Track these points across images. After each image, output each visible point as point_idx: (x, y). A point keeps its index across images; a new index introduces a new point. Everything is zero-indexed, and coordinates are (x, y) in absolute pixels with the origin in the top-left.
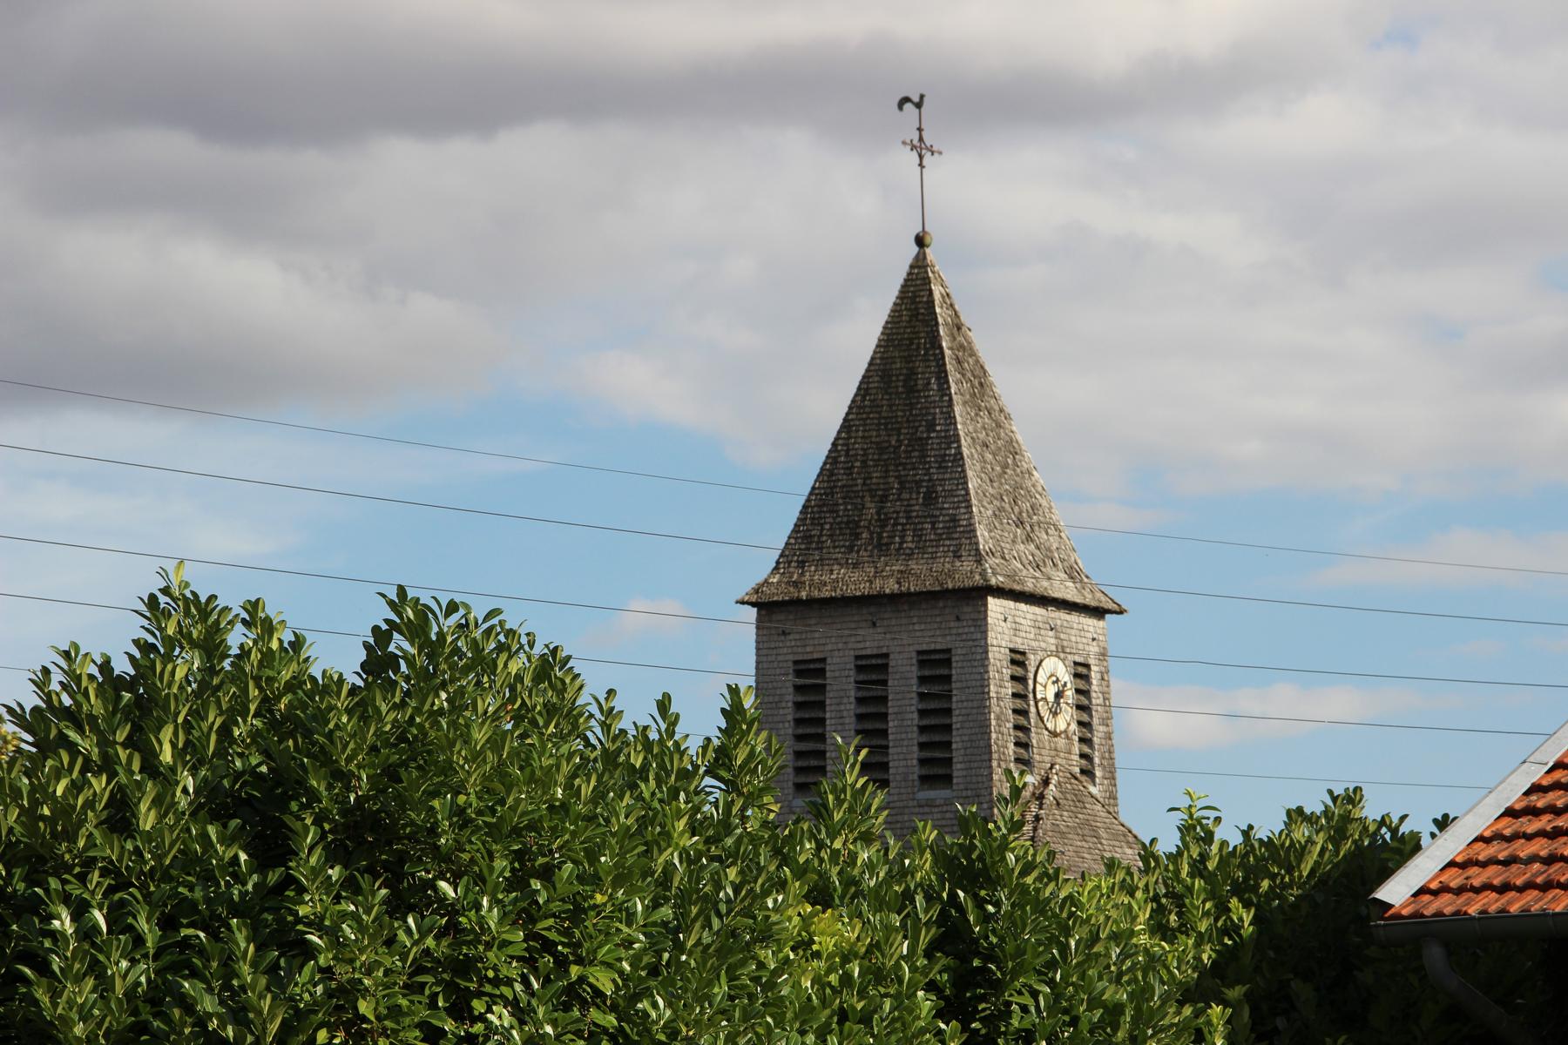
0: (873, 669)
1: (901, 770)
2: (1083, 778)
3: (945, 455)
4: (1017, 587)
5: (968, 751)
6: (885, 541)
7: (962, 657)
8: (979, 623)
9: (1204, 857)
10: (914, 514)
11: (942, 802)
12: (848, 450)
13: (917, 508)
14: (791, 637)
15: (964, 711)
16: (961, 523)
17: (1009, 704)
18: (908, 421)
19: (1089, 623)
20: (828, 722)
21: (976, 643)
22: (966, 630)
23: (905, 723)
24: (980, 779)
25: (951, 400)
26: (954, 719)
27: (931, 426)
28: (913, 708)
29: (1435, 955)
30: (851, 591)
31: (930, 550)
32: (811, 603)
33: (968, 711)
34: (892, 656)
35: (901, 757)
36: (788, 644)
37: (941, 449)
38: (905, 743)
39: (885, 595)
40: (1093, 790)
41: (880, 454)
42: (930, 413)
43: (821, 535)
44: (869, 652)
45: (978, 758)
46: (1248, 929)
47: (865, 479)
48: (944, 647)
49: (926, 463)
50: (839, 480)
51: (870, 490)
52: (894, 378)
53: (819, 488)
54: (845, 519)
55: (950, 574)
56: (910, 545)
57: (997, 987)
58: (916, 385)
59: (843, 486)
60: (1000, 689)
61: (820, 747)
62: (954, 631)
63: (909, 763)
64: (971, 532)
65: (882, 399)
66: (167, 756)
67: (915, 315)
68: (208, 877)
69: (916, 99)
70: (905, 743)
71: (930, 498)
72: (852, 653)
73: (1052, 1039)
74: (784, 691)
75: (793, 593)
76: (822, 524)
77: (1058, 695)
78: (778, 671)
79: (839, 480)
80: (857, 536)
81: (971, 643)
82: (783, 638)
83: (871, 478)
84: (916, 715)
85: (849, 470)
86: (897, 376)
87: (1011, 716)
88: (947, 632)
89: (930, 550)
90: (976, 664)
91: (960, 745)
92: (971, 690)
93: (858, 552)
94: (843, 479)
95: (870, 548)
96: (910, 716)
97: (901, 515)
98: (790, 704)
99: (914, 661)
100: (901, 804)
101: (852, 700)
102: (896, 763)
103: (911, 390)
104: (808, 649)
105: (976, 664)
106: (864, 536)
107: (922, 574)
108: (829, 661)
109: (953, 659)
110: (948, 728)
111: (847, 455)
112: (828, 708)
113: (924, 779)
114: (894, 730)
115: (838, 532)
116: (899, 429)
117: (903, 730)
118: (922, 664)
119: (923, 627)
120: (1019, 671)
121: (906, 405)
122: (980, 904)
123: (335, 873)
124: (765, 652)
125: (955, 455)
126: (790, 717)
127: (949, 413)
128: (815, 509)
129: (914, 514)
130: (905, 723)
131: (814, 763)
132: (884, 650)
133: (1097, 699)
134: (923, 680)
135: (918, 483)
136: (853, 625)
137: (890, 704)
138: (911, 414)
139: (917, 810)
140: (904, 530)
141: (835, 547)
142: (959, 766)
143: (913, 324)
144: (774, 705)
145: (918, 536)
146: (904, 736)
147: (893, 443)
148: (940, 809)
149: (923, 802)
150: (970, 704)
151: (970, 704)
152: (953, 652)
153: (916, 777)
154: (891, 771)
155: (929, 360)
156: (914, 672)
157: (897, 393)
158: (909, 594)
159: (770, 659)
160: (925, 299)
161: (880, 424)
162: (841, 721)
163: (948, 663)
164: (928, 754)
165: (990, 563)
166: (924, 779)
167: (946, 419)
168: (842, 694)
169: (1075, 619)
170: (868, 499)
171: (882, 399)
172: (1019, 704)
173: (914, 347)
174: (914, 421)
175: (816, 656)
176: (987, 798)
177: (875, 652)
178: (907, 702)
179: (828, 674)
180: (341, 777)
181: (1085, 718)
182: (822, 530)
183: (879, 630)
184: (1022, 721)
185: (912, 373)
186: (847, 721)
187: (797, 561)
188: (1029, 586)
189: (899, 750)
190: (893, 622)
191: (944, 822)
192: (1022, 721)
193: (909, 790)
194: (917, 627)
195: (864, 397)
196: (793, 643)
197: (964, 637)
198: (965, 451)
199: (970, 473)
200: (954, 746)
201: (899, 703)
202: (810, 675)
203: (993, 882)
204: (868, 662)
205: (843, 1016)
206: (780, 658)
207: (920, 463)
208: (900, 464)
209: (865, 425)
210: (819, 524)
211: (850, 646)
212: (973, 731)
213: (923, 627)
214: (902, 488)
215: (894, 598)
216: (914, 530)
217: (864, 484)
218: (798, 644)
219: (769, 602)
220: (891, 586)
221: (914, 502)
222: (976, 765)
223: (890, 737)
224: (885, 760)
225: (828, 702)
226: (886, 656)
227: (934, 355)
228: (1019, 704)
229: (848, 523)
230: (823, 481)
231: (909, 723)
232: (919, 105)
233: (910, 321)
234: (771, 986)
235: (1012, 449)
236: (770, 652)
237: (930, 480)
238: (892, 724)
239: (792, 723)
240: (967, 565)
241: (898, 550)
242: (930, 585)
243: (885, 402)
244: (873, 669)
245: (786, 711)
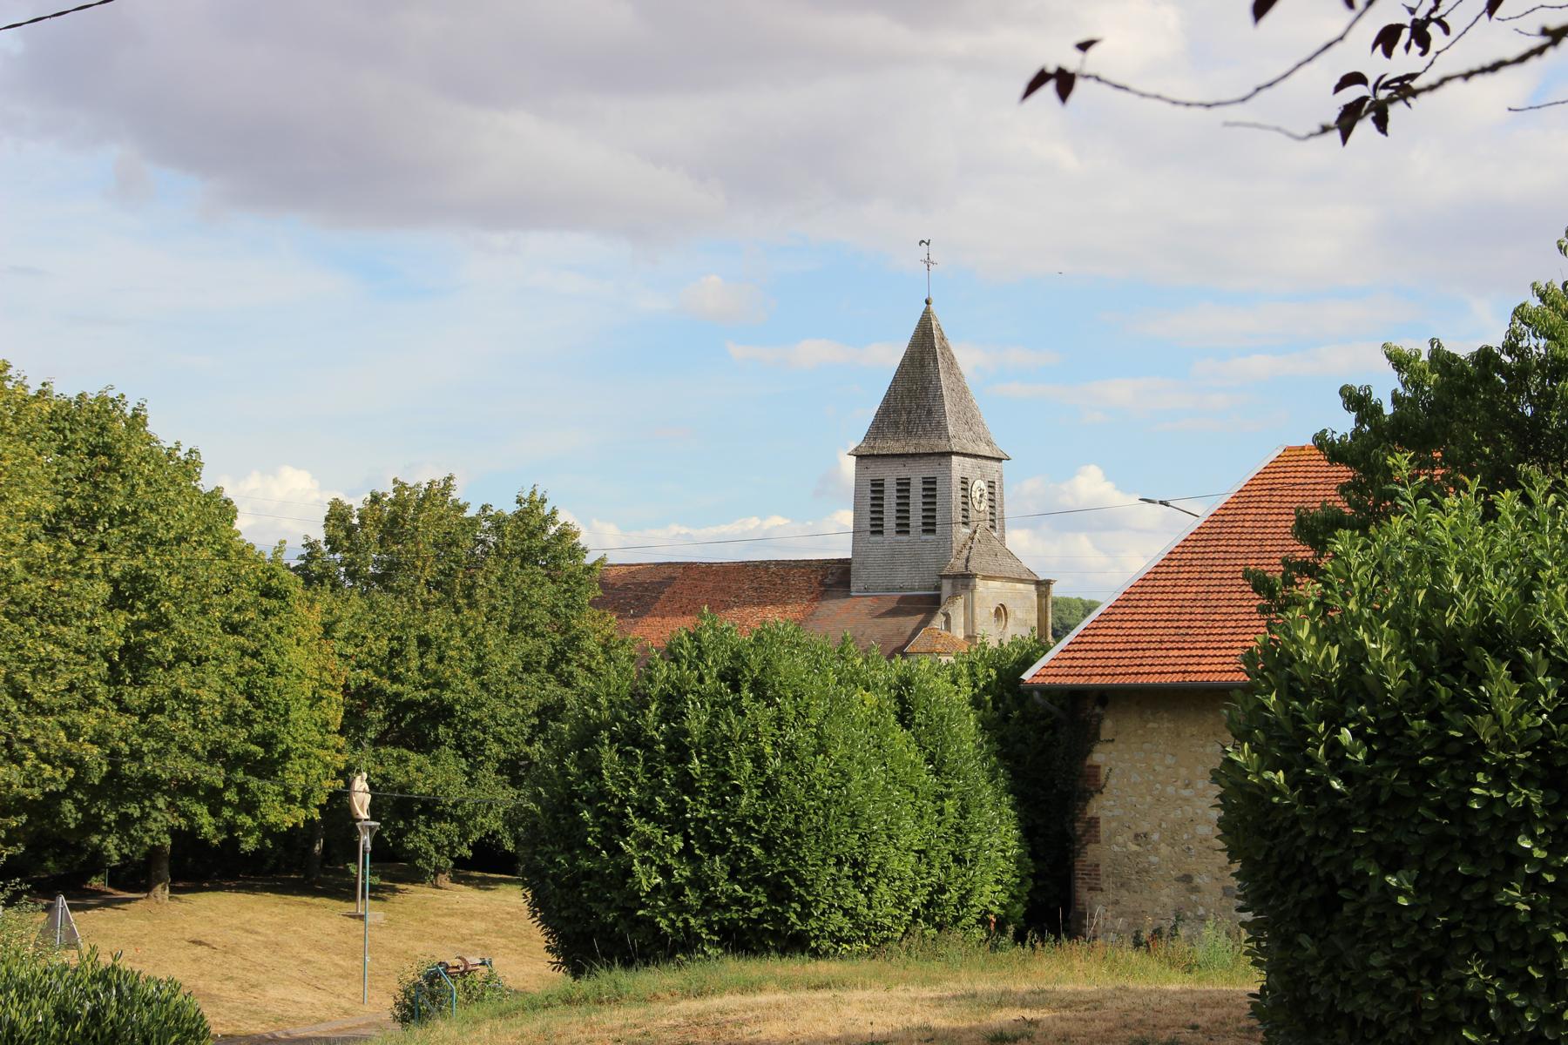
0: (904, 486)
2: (991, 530)
4: (964, 451)
9: (984, 654)
17: (960, 499)
19: (995, 464)
27: (930, 382)
29: (1036, 694)
32: (878, 456)
40: (995, 534)
46: (994, 677)
55: (937, 446)
57: (912, 712)
60: (957, 495)
61: (881, 516)
64: (946, 428)
66: (710, 664)
67: (924, 333)
68: (721, 694)
71: (929, 412)
77: (981, 496)
80: (898, 428)
87: (961, 505)
103: (923, 366)
107: (925, 445)
120: (965, 486)
122: (908, 690)
123: (751, 695)
131: (878, 522)
133: (997, 497)
134: (924, 489)
135: (924, 406)
145: (924, 429)
156: (921, 486)
163: (935, 483)
164: (926, 521)
165: (953, 441)
166: (924, 531)
169: (989, 463)
172: (964, 500)
180: (751, 671)
181: (992, 504)
184: (965, 507)
185: (923, 359)
188: (969, 451)
192: (965, 507)
198: (944, 393)
199: (946, 403)
202: (878, 486)
203: (911, 684)
205: (871, 724)
215: (913, 455)
220: (912, 450)
228: (964, 500)
232: (928, 244)
234: (853, 719)
235: (965, 391)
240: (944, 442)
242: (928, 450)
244: (904, 486)
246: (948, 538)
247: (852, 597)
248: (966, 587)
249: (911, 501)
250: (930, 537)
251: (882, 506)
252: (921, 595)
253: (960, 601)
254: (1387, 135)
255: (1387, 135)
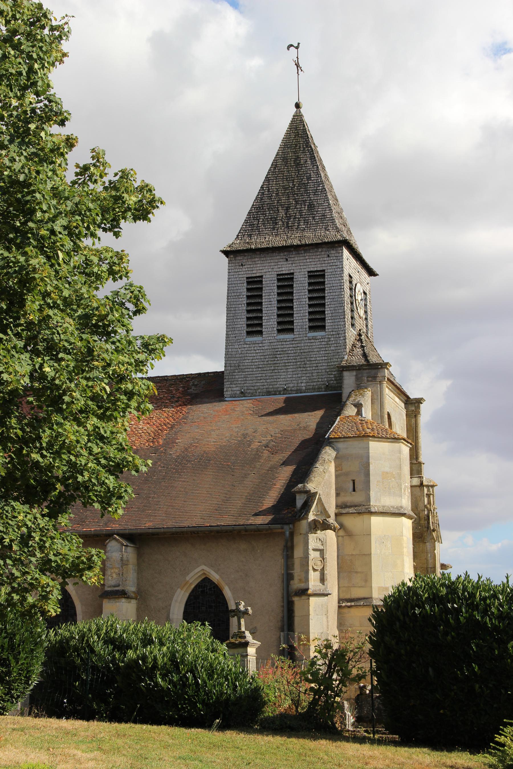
1: (299, 324)
3: (317, 189)
5: (333, 315)
6: (290, 225)
7: (330, 273)
8: (339, 258)
10: (304, 214)
11: (320, 337)
12: (269, 189)
13: (305, 211)
14: (246, 267)
15: (331, 297)
16: (327, 216)
18: (297, 177)
20: (263, 304)
21: (337, 267)
22: (332, 261)
23: (302, 303)
24: (339, 326)
25: (318, 167)
26: (326, 301)
27: (309, 178)
28: (306, 296)
30: (277, 244)
31: (313, 228)
33: (333, 297)
34: (295, 274)
35: (300, 318)
36: (244, 270)
37: (315, 187)
38: (302, 312)
39: (294, 245)
41: (285, 190)
42: (308, 173)
43: (258, 224)
44: (284, 272)
45: (338, 317)
47: (278, 201)
48: (321, 269)
49: (307, 193)
50: (265, 201)
51: (281, 205)
52: (289, 160)
53: (256, 205)
54: (270, 217)
56: (303, 226)
58: (300, 162)
59: (268, 204)
61: (259, 315)
62: (327, 262)
63: (304, 321)
65: (284, 169)
67: (297, 135)
69: (296, 45)
70: (302, 312)
71: (311, 207)
72: (276, 273)
73: (2, 630)
74: (242, 291)
75: (248, 247)
76: (258, 220)
78: (239, 282)
79: (265, 201)
80: (276, 224)
81: (335, 267)
82: (241, 267)
83: (281, 200)
84: (307, 299)
85: (270, 197)
86: (290, 159)
88: (323, 262)
89: (313, 228)
90: (337, 276)
91: (329, 312)
92: (335, 288)
93: (277, 230)
94: (266, 200)
95: (283, 228)
96: (305, 300)
97: (297, 214)
98: (245, 296)
99: (307, 276)
100: (300, 339)
101: (276, 293)
102: (298, 321)
103: (298, 164)
104: (254, 272)
105: (337, 276)
106: (280, 223)
108: (264, 277)
109: (326, 274)
110: (324, 305)
111: (269, 191)
112: (263, 298)
113: (311, 328)
114: (296, 306)
115: (266, 222)
116: (293, 180)
117: (301, 306)
118: (310, 277)
119: (311, 260)
121: (296, 170)
124: (232, 274)
125: (322, 189)
126: (245, 302)
127: (317, 172)
128: (255, 214)
129: (304, 214)
130: (302, 303)
132: (292, 271)
136: (276, 261)
137: (294, 295)
138: (299, 174)
139: (308, 341)
140: (299, 220)
141: (265, 228)
142: (329, 321)
143: (296, 138)
144: (237, 297)
145: (306, 222)
146: (301, 309)
147: (291, 186)
148: (319, 340)
149: (311, 338)
150: (334, 294)
151: (334, 294)
152: (326, 271)
153: (307, 327)
154: (295, 324)
155: (305, 152)
157: (291, 166)
158: (306, 245)
159: (235, 276)
160: (302, 128)
161: (283, 178)
162: (270, 303)
163: (323, 276)
167: (316, 175)
168: (271, 291)
170: (280, 208)
171: (284, 169)
173: (298, 147)
174: (300, 177)
175: (258, 275)
176: (343, 335)
177: (287, 272)
178: (303, 294)
179: (264, 283)
182: (259, 222)
183: (289, 262)
186: (273, 303)
187: (248, 235)
189: (299, 315)
190: (296, 259)
191: (321, 346)
193: (304, 332)
194: (308, 261)
195: (275, 168)
196: (246, 269)
197: (331, 264)
200: (326, 312)
201: (299, 294)
204: (284, 277)
206: (239, 276)
207: (305, 193)
208: (295, 194)
209: (277, 179)
210: (257, 219)
211: (275, 270)
212: (336, 305)
213: (311, 260)
214: (297, 202)
216: (304, 220)
217: (278, 203)
218: (249, 269)
219: (236, 251)
220: (296, 242)
221: (303, 209)
222: (337, 320)
223: (295, 309)
224: (292, 320)
225: (264, 295)
226: (293, 274)
227: (308, 150)
229: (271, 218)
230: (257, 202)
231: (304, 303)
232: (297, 48)
233: (295, 137)
236: (235, 273)
237: (310, 200)
238: (295, 304)
239: (246, 305)
241: (297, 229)
243: (285, 170)
245: (242, 299)
246: (341, 334)
247: (226, 401)
248: (374, 378)
249: (295, 297)
250: (319, 334)
251: (261, 304)
252: (311, 396)
253: (368, 394)
254: (377, 275)
255: (377, 275)
